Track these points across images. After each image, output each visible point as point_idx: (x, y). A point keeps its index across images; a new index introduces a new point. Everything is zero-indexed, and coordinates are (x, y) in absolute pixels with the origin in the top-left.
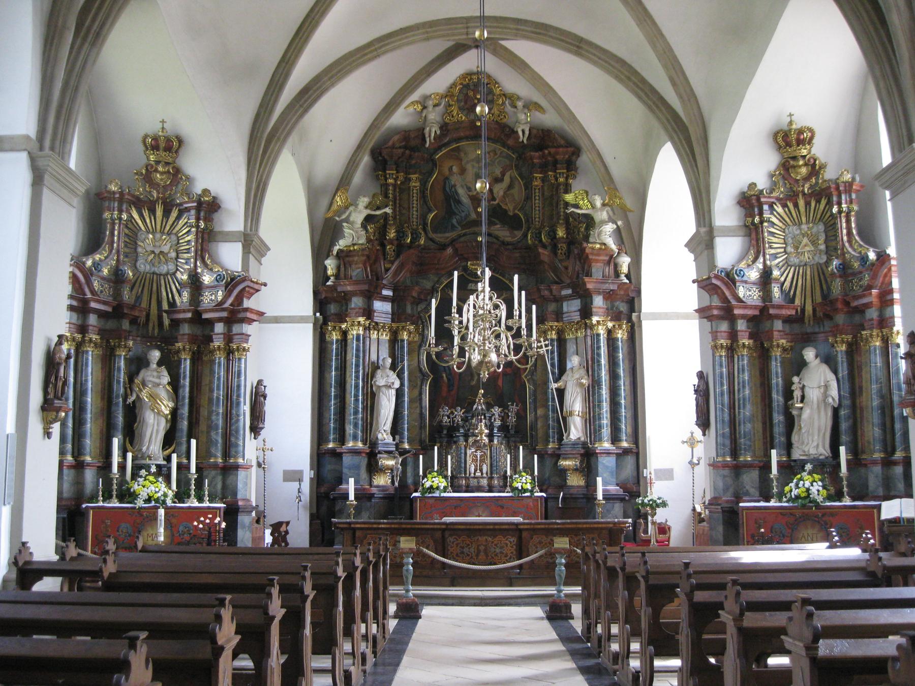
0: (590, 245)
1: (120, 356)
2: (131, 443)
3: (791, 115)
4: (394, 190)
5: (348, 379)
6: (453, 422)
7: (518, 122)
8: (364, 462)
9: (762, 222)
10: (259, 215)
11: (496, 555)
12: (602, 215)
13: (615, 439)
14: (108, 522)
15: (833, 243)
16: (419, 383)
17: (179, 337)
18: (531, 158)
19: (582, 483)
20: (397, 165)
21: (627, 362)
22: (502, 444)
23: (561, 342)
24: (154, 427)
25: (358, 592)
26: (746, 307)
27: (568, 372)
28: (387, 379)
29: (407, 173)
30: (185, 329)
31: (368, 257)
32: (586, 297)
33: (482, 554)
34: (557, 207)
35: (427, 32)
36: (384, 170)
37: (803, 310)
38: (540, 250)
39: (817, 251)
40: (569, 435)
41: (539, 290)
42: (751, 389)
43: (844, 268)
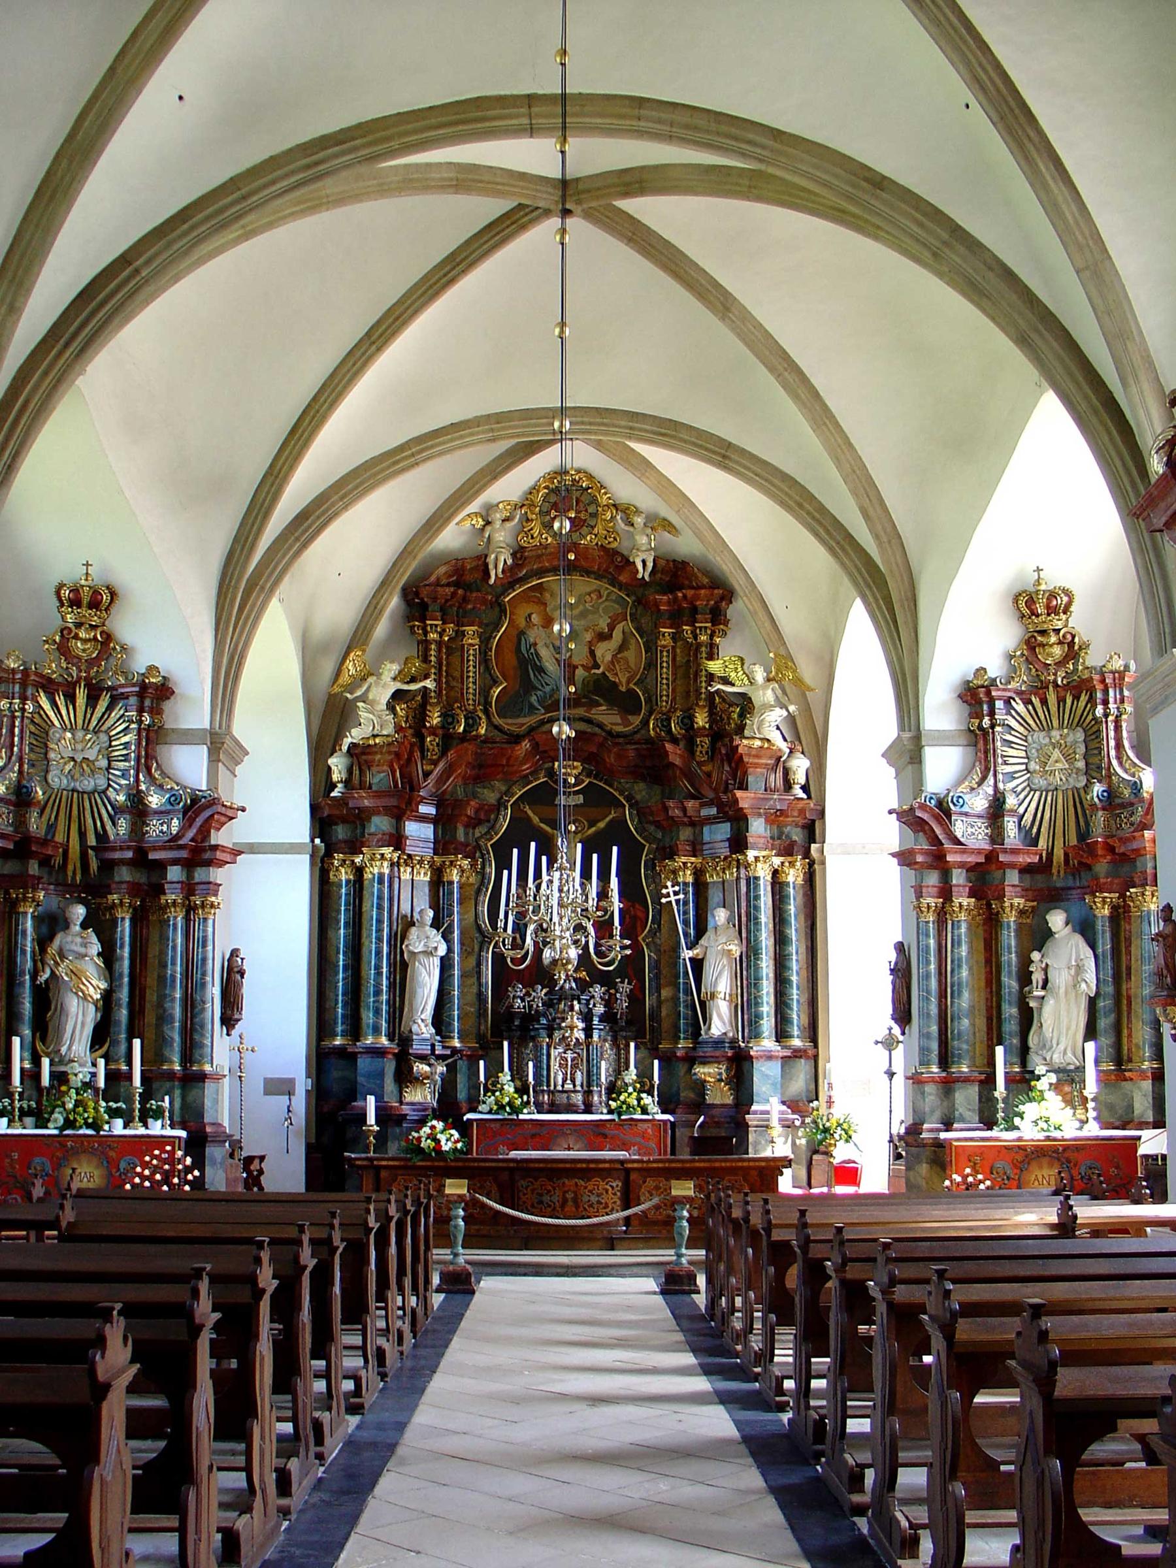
0: (745, 742)
1: (26, 913)
2: (43, 1040)
3: (1038, 570)
4: (439, 650)
5: (364, 940)
6: (531, 1007)
7: (635, 547)
8: (390, 1066)
9: (993, 726)
11: (591, 1206)
12: (765, 695)
13: (781, 1035)
14: (16, 1156)
15: (1096, 760)
16: (476, 949)
17: (114, 886)
18: (657, 604)
19: (729, 1100)
21: (802, 918)
22: (605, 1040)
23: (700, 887)
25: (393, 1250)
27: (710, 933)
29: (459, 624)
30: (124, 874)
31: (398, 755)
32: (739, 821)
33: (570, 1203)
34: (695, 680)
35: (492, 430)
36: (423, 619)
37: (1050, 854)
38: (669, 746)
39: (1072, 771)
40: (709, 1028)
41: (666, 809)
42: (970, 969)
43: (1109, 797)
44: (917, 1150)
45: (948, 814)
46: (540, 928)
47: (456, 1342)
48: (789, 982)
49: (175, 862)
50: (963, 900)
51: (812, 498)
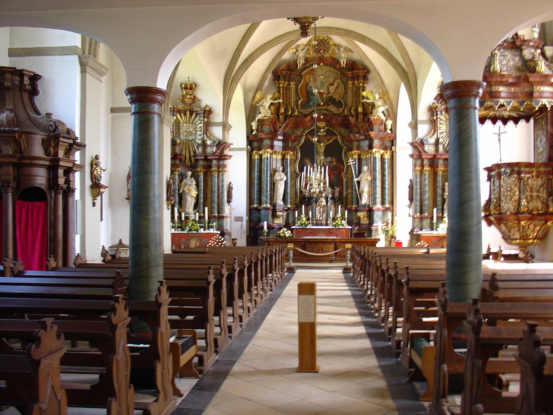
2: (181, 208)
4: (283, 90)
8: (270, 213)
9: (437, 119)
10: (228, 114)
12: (379, 103)
13: (383, 203)
14: (177, 238)
18: (347, 75)
19: (367, 222)
20: (284, 77)
21: (389, 169)
24: (190, 202)
29: (289, 81)
30: (201, 163)
31: (272, 122)
32: (371, 140)
36: (279, 80)
38: (350, 118)
41: (350, 137)
42: (429, 187)
44: (415, 237)
45: (423, 144)
46: (311, 185)
47: (291, 281)
49: (215, 159)
50: (427, 168)
51: (388, 52)
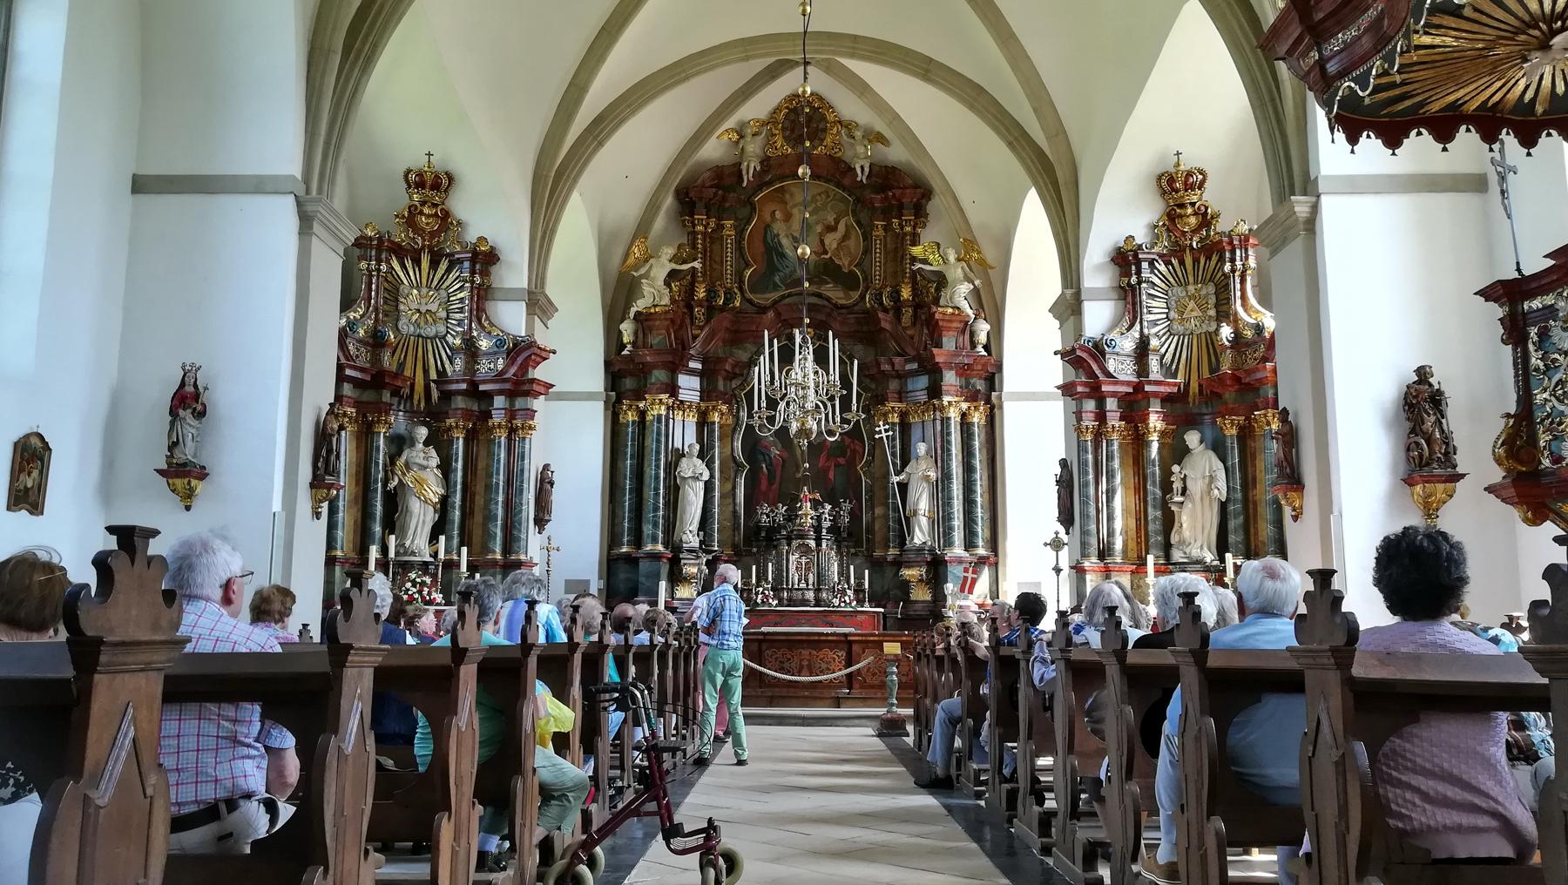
3: (1178, 154)
4: (704, 240)
7: (856, 156)
8: (665, 569)
9: (1139, 283)
12: (955, 272)
13: (969, 544)
19: (928, 597)
23: (905, 427)
24: (420, 516)
26: (1117, 383)
27: (913, 462)
28: (693, 467)
29: (719, 219)
30: (460, 402)
31: (672, 321)
32: (934, 372)
36: (692, 215)
37: (1187, 385)
38: (881, 315)
41: (878, 364)
45: (1103, 354)
48: (975, 502)
49: (500, 392)
50: (1114, 420)
